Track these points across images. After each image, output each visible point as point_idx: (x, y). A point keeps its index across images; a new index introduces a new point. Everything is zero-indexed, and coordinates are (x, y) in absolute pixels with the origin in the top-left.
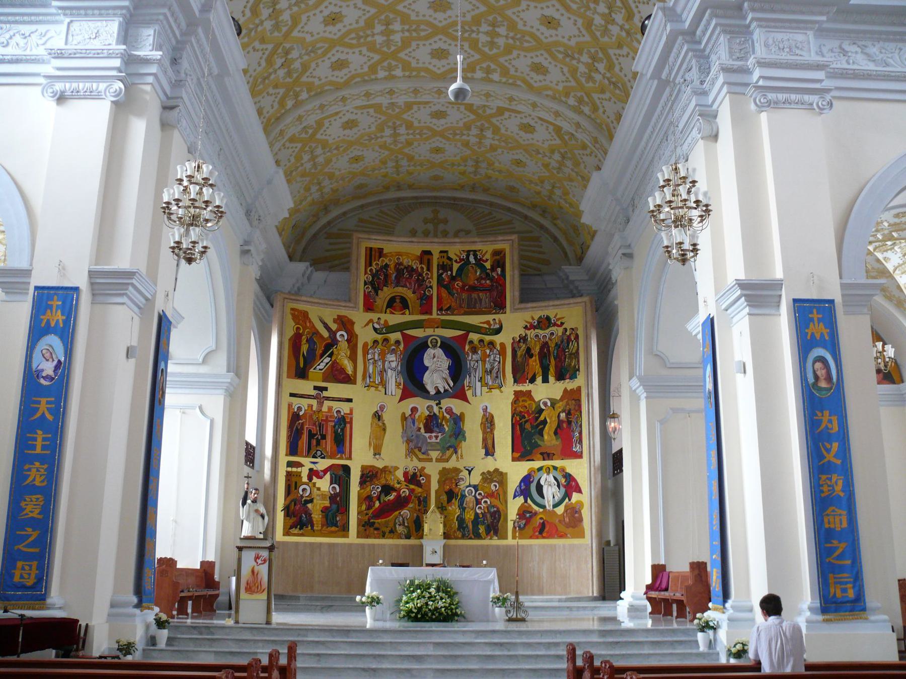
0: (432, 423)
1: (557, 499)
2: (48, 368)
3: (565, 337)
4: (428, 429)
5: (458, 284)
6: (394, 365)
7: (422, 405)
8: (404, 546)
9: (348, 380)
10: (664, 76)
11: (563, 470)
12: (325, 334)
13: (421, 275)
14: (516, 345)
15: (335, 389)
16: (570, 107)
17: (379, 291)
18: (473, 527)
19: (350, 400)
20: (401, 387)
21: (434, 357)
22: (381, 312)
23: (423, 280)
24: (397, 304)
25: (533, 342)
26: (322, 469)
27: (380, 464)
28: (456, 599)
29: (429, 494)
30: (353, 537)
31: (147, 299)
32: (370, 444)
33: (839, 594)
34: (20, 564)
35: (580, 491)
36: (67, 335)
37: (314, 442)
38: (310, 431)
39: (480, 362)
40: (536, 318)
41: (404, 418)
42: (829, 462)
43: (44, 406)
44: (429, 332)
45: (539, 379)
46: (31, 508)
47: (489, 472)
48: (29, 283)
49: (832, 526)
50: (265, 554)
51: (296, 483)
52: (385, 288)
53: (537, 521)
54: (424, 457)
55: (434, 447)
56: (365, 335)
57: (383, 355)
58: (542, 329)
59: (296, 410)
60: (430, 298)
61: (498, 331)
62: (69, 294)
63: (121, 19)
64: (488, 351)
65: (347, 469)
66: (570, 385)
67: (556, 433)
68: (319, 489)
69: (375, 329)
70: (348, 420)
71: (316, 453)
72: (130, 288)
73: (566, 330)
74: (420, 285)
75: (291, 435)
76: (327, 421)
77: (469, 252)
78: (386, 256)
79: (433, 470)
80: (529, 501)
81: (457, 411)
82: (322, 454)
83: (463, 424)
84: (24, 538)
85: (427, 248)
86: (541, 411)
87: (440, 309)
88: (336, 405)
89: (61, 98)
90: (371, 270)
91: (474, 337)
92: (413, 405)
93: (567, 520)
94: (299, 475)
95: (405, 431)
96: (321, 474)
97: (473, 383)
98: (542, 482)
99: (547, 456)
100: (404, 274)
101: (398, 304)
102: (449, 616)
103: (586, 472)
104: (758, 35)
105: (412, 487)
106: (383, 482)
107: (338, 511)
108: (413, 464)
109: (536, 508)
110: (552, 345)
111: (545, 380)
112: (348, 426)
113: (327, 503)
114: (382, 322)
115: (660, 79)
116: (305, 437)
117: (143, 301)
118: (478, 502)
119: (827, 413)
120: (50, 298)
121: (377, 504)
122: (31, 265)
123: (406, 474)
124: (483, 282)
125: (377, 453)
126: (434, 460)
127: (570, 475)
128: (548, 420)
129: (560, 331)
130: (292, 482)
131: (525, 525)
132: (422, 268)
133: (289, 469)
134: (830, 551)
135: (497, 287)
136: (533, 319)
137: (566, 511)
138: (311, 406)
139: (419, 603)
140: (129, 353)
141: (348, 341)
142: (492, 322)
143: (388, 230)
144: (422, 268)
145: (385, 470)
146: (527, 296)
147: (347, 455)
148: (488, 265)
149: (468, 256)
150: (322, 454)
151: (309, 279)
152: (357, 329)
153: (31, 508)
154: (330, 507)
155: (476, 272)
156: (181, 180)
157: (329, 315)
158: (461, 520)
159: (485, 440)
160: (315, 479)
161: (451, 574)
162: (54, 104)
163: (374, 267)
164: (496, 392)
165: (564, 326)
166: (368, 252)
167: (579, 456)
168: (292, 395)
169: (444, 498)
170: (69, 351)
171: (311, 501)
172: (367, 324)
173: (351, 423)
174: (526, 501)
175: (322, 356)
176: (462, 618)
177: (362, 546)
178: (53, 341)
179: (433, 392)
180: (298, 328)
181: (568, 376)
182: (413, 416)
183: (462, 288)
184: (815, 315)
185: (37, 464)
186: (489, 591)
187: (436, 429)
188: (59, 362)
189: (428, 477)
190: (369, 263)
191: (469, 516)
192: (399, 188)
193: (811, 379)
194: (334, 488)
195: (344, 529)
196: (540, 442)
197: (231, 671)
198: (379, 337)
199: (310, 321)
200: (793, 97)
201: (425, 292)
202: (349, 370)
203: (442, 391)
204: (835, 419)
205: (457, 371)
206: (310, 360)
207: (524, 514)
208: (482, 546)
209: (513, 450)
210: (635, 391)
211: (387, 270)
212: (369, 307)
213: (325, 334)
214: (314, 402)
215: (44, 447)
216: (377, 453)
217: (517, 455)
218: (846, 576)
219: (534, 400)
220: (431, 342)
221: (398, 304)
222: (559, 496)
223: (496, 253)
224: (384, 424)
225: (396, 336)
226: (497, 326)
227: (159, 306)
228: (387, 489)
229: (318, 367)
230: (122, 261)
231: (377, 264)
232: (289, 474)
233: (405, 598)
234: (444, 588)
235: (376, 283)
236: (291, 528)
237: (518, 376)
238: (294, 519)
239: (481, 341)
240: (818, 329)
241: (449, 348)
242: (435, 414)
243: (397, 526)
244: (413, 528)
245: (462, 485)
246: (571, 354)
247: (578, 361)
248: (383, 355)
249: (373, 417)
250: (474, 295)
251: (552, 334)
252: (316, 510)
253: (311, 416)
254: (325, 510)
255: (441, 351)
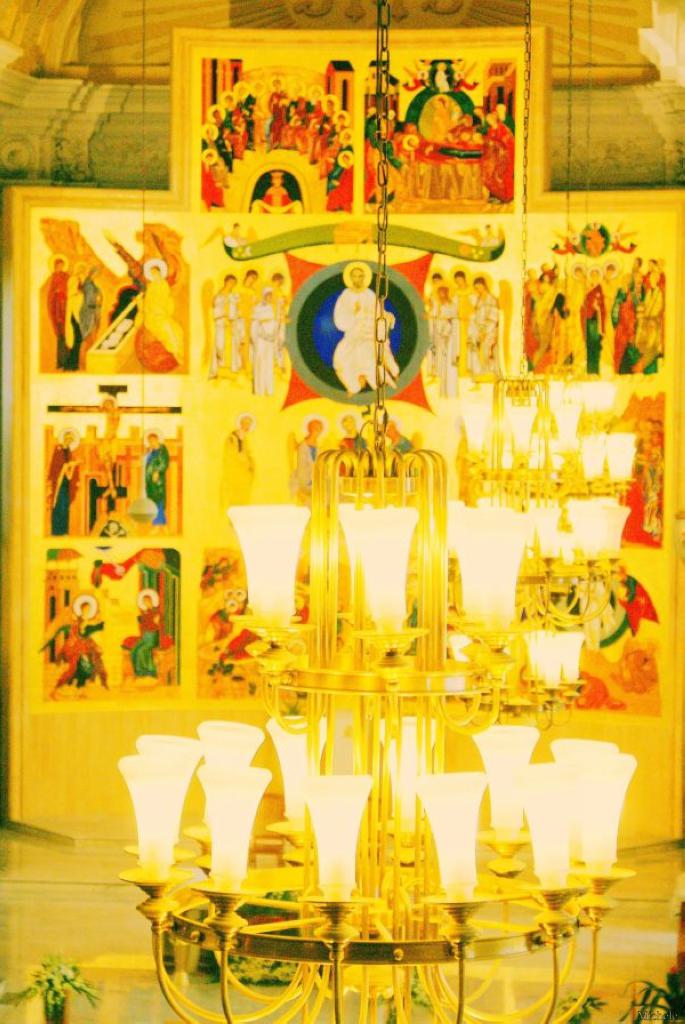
1: (608, 631)
3: (638, 279)
5: (409, 141)
6: (270, 328)
14: (533, 288)
21: (358, 309)
22: (241, 210)
35: (654, 617)
37: (103, 504)
38: (93, 483)
40: (579, 228)
51: (67, 593)
52: (248, 154)
56: (204, 263)
60: (346, 175)
65: (172, 557)
68: (115, 602)
70: (172, 452)
71: (107, 528)
73: (640, 262)
74: (326, 145)
75: (52, 496)
76: (127, 456)
77: (434, 63)
82: (120, 528)
88: (149, 423)
90: (216, 114)
92: (310, 418)
93: (627, 675)
96: (120, 570)
101: (277, 190)
107: (156, 644)
110: (610, 294)
112: (173, 465)
113: (134, 630)
116: (82, 496)
127: (635, 583)
129: (624, 263)
132: (331, 103)
135: (496, 151)
137: (626, 657)
142: (483, 233)
144: (331, 103)
148: (477, 97)
149: (433, 74)
150: (120, 528)
152: (189, 251)
154: (141, 638)
155: (450, 113)
163: (223, 107)
165: (637, 253)
166: (209, 71)
168: (53, 409)
171: (100, 627)
172: (211, 239)
173: (179, 459)
180: (59, 262)
182: (311, 441)
183: (419, 152)
194: (147, 597)
198: (239, 269)
199: (84, 244)
201: (336, 159)
202: (173, 346)
205: (405, 340)
211: (251, 111)
214: (100, 421)
220: (351, 273)
221: (277, 190)
223: (497, 69)
224: (250, 459)
229: (107, 344)
231: (230, 98)
232: (52, 576)
237: (538, 356)
238: (63, 668)
246: (648, 319)
247: (663, 336)
250: (446, 168)
251: (611, 268)
253: (94, 451)
254: (129, 643)
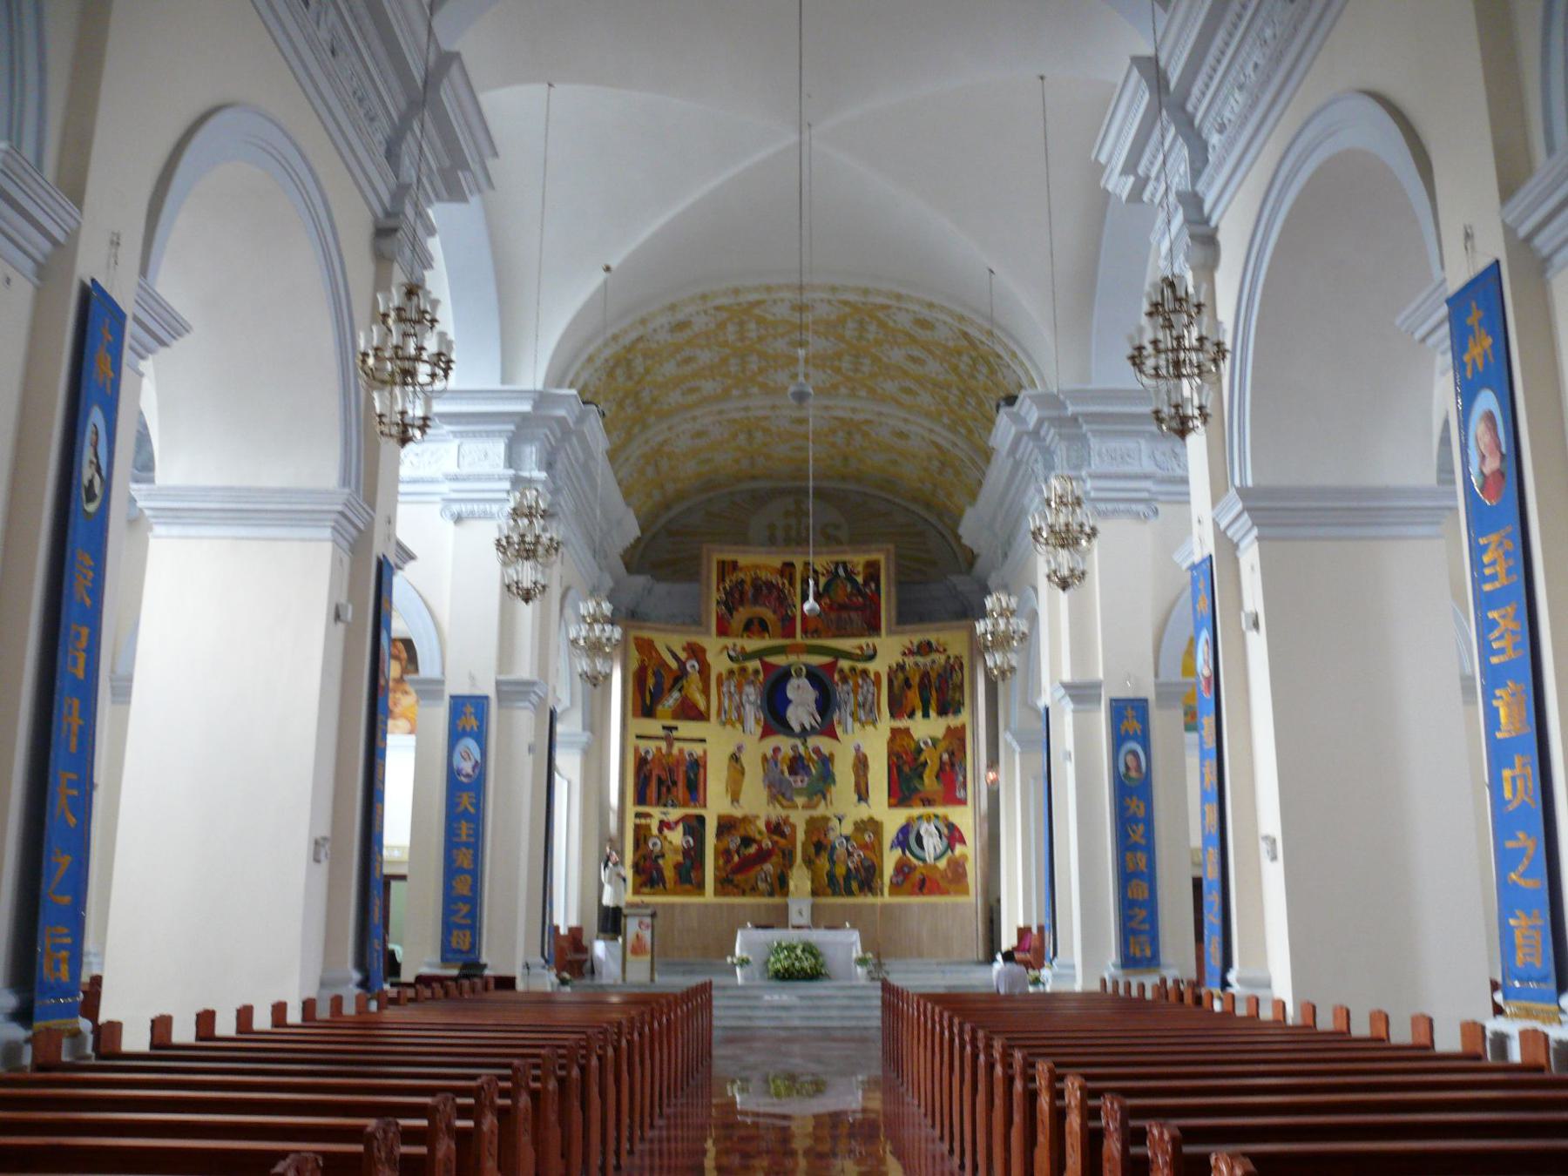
0: (797, 764)
1: (938, 851)
2: (467, 767)
3: (948, 667)
4: (793, 771)
6: (752, 698)
7: (786, 744)
8: (767, 906)
9: (701, 716)
10: (1141, 171)
11: (945, 819)
12: (674, 664)
13: (782, 591)
15: (686, 728)
16: (944, 426)
17: (735, 613)
18: (845, 882)
19: (703, 741)
20: (762, 724)
23: (785, 598)
24: (755, 627)
25: (912, 671)
26: (674, 820)
27: (738, 813)
28: (821, 959)
29: (794, 846)
30: (709, 895)
31: (55, 242)
32: (727, 790)
33: (1138, 954)
34: (455, 933)
36: (481, 737)
37: (664, 789)
39: (852, 695)
40: (916, 642)
41: (765, 759)
42: (1136, 843)
43: (466, 800)
44: (792, 658)
45: (919, 714)
46: (462, 888)
47: (862, 821)
48: (442, 691)
49: (1135, 897)
50: (648, 920)
51: (645, 837)
52: (741, 609)
53: (917, 876)
54: (789, 803)
55: (800, 792)
56: (719, 664)
57: (739, 687)
58: (921, 655)
59: (643, 754)
61: (871, 657)
62: (480, 703)
63: (506, 441)
64: (860, 681)
65: (701, 820)
66: (953, 721)
67: (937, 777)
68: (671, 843)
69: (730, 656)
70: (701, 763)
72: (532, 695)
73: (949, 657)
77: (837, 564)
78: (741, 569)
79: (799, 818)
80: (907, 852)
81: (825, 751)
83: (833, 764)
84: (456, 912)
85: (788, 558)
86: (920, 751)
87: (805, 631)
88: (687, 747)
89: (458, 519)
90: (724, 588)
91: (845, 664)
93: (950, 875)
94: (648, 827)
95: (766, 775)
96: (673, 825)
97: (842, 717)
98: (922, 832)
99: (927, 802)
100: (763, 591)
101: (756, 627)
102: (814, 975)
103: (971, 821)
104: (1094, 443)
105: (776, 838)
106: (742, 832)
108: (776, 812)
109: (914, 861)
110: (933, 675)
111: (926, 715)
112: (702, 771)
113: (680, 858)
114: (738, 648)
115: (1136, 175)
117: (47, 246)
118: (850, 854)
119: (1135, 798)
120: (463, 705)
121: (736, 858)
122: (443, 673)
123: (768, 824)
124: (854, 599)
125: (735, 799)
126: (800, 808)
128: (929, 761)
129: (941, 659)
130: (641, 835)
131: (903, 881)
132: (783, 584)
133: (638, 821)
134: (1131, 918)
136: (912, 643)
138: (659, 749)
139: (786, 964)
140: (531, 749)
141: (700, 672)
142: (865, 648)
143: (741, 538)
145: (745, 820)
146: (908, 616)
147: (701, 802)
148: (860, 579)
149: (836, 568)
151: (650, 592)
152: (710, 657)
153: (462, 888)
156: (385, 316)
157: (678, 642)
158: (831, 876)
159: (857, 785)
160: (666, 831)
161: (818, 936)
162: (452, 523)
164: (869, 728)
167: (963, 802)
168: (638, 737)
169: (812, 850)
170: (484, 753)
172: (721, 652)
174: (904, 852)
175: (670, 690)
176: (827, 977)
177: (720, 906)
178: (469, 744)
179: (797, 729)
180: (643, 661)
181: (951, 711)
184: (1130, 713)
185: (464, 849)
186: (851, 953)
187: (801, 771)
188: (477, 762)
189: (793, 827)
190: (721, 579)
191: (840, 871)
192: (754, 478)
193: (1122, 769)
194: (688, 842)
195: (700, 887)
196: (919, 787)
197: (450, 1095)
198: (735, 666)
199: (657, 651)
200: (1122, 506)
202: (702, 705)
203: (808, 727)
204: (1142, 805)
205: (825, 704)
206: (657, 696)
207: (902, 869)
208: (855, 906)
209: (890, 795)
210: (1225, 532)
212: (723, 631)
213: (674, 664)
215: (469, 835)
216: (735, 799)
217: (892, 801)
218: (1143, 938)
219: (913, 740)
221: (756, 627)
222: (940, 847)
225: (754, 664)
226: (871, 652)
227: (550, 703)
228: (747, 841)
230: (524, 669)
232: (637, 828)
233: (772, 959)
234: (809, 949)
235: (731, 602)
236: (641, 886)
238: (644, 877)
239: (853, 669)
240: (1132, 725)
241: (817, 678)
242: (800, 755)
243: (759, 883)
244: (777, 886)
245: (832, 836)
248: (739, 687)
249: (730, 760)
250: (844, 615)
252: (668, 866)
253: (660, 760)
255: (806, 681)
